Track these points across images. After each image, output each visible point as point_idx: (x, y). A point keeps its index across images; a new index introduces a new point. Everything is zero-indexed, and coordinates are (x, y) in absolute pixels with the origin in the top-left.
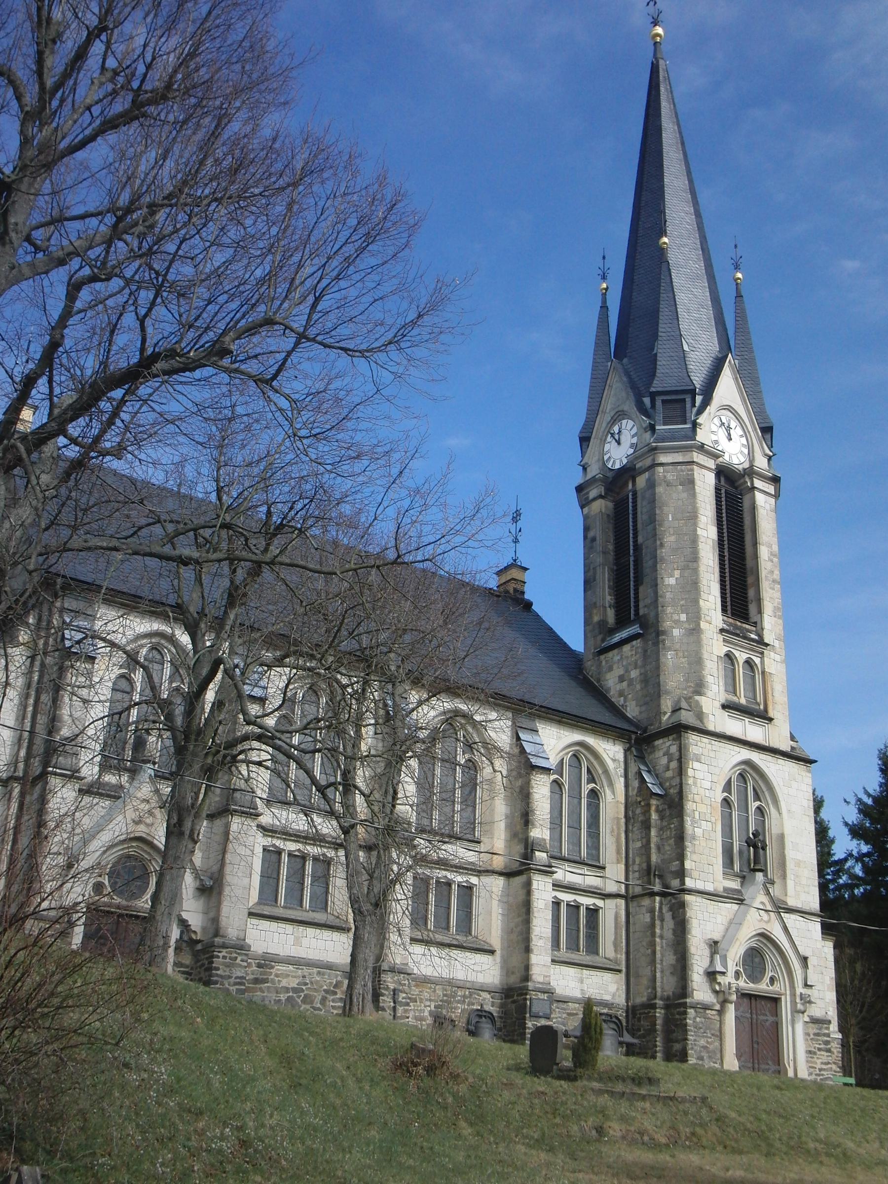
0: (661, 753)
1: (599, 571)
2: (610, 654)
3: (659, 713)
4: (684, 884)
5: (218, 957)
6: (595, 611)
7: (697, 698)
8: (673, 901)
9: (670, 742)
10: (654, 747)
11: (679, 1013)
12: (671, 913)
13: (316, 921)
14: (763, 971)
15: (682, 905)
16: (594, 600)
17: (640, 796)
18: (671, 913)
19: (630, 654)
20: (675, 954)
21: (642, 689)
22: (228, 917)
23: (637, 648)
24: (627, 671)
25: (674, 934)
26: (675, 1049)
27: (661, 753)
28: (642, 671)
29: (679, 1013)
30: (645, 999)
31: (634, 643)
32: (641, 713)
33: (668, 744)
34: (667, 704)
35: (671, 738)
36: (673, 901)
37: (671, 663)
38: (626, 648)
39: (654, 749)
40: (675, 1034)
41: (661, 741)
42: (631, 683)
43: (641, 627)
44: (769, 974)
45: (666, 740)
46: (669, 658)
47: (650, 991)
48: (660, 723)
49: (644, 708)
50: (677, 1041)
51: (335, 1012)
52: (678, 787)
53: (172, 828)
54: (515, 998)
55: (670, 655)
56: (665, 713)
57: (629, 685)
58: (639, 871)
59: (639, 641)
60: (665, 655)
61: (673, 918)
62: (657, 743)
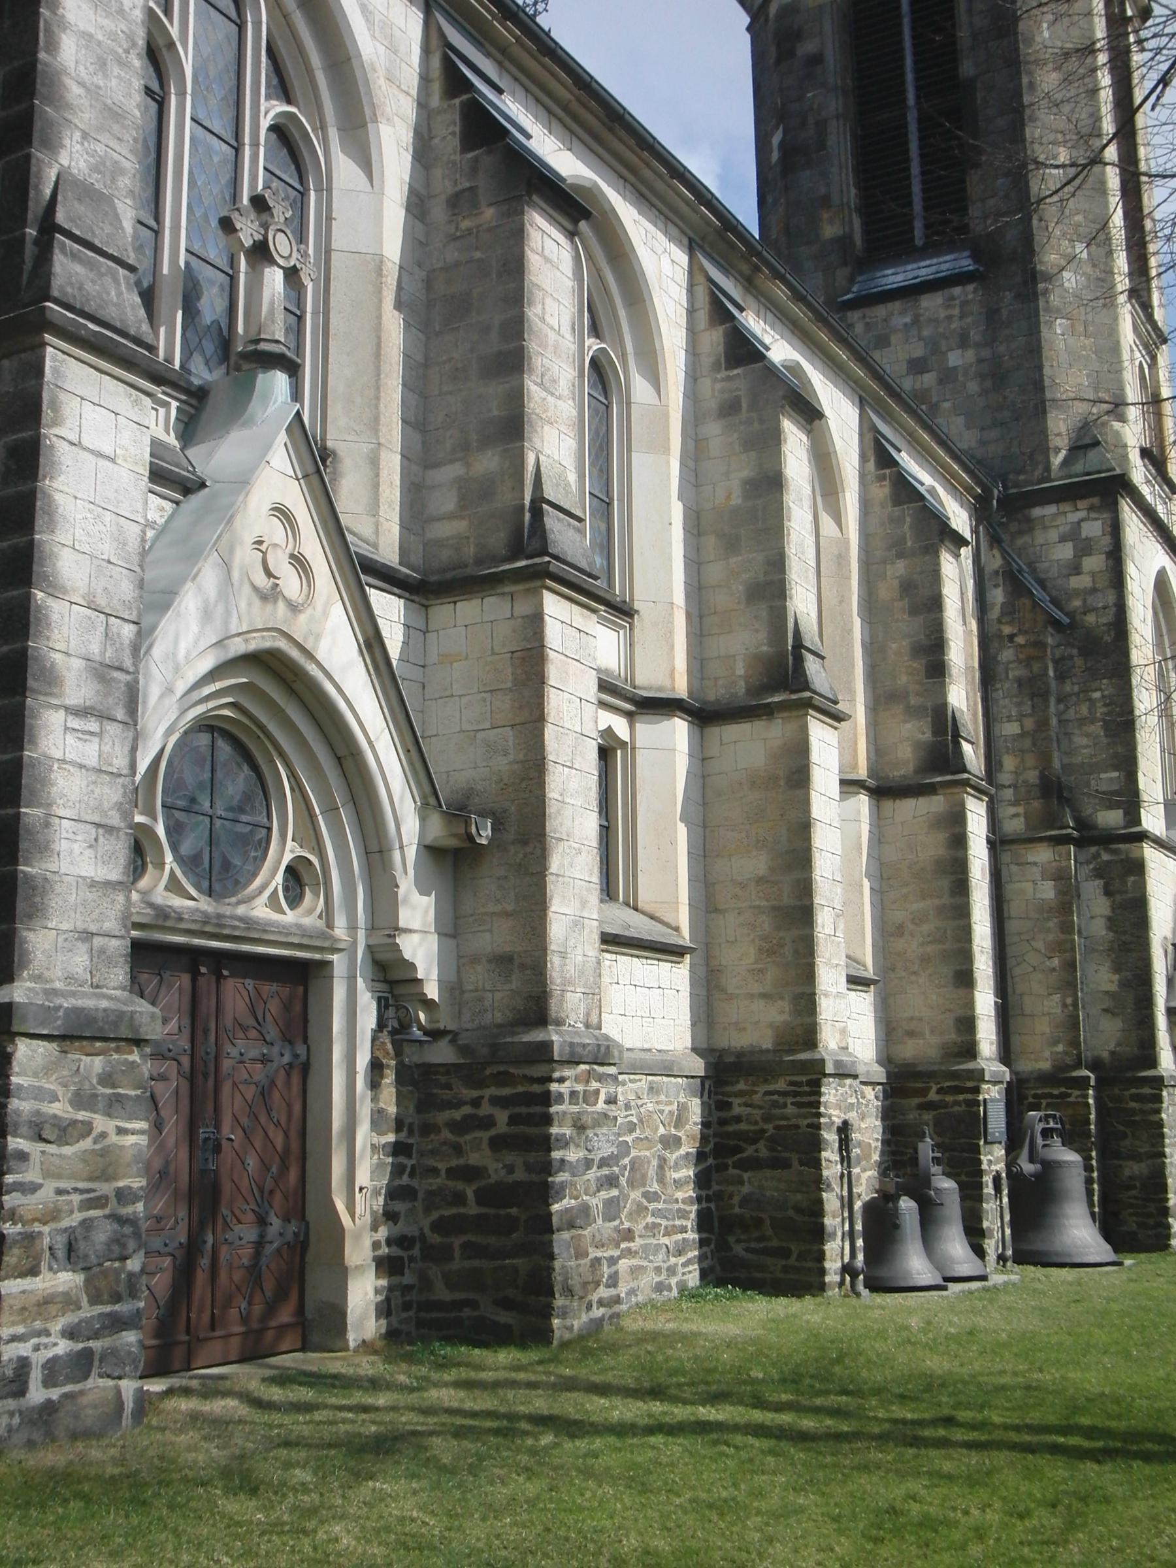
0: (1053, 535)
1: (833, 126)
2: (881, 311)
3: (1043, 449)
4: (1138, 822)
5: (560, 1098)
6: (825, 216)
7: (1116, 425)
8: (1106, 857)
9: (1082, 514)
10: (1029, 520)
11: (1137, 1098)
12: (1099, 883)
13: (632, 933)
14: (256, 844)
15: (1138, 868)
16: (823, 190)
17: (1010, 623)
18: (1099, 883)
19: (943, 314)
20: (1117, 968)
21: (985, 392)
22: (563, 955)
23: (965, 303)
24: (935, 348)
25: (1110, 929)
26: (1127, 1172)
27: (1053, 535)
28: (986, 353)
29: (1137, 1098)
30: (1045, 1065)
31: (957, 291)
32: (983, 443)
33: (1073, 517)
34: (1060, 428)
35: (1082, 504)
36: (1106, 857)
37: (1062, 345)
38: (931, 303)
39: (1029, 525)
40: (1127, 1142)
41: (1051, 510)
42: (947, 377)
43: (976, 256)
44: (285, 850)
45: (1066, 507)
46: (1058, 335)
47: (1060, 1048)
48: (1048, 468)
49: (994, 434)
50: (1136, 1157)
51: (680, 1195)
52: (1112, 611)
53: (992, 629)
54: (933, 1096)
55: (1060, 325)
56: (1058, 450)
57: (941, 382)
58: (1014, 786)
59: (970, 288)
60: (1051, 324)
61: (1108, 893)
62: (1037, 512)
